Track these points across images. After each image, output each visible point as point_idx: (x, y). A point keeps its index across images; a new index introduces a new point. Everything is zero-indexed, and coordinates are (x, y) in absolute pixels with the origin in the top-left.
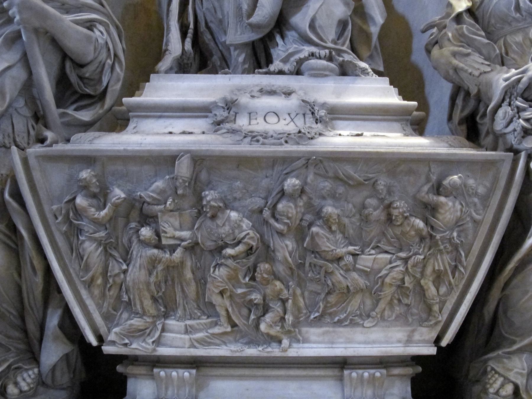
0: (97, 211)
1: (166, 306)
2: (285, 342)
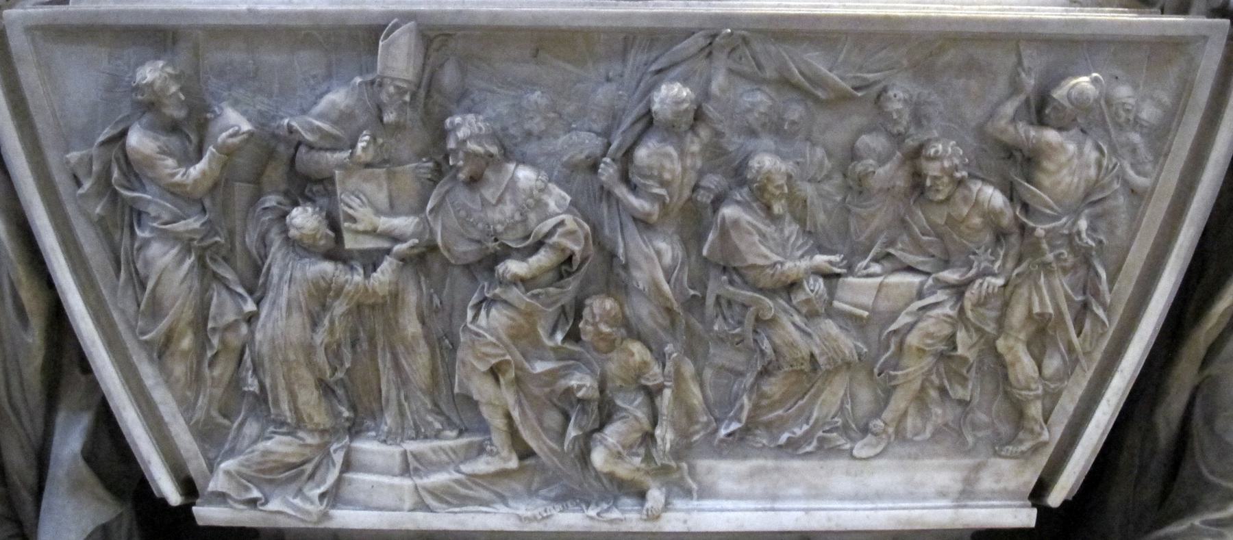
0: (180, 166)
1: (355, 405)
2: (656, 496)
